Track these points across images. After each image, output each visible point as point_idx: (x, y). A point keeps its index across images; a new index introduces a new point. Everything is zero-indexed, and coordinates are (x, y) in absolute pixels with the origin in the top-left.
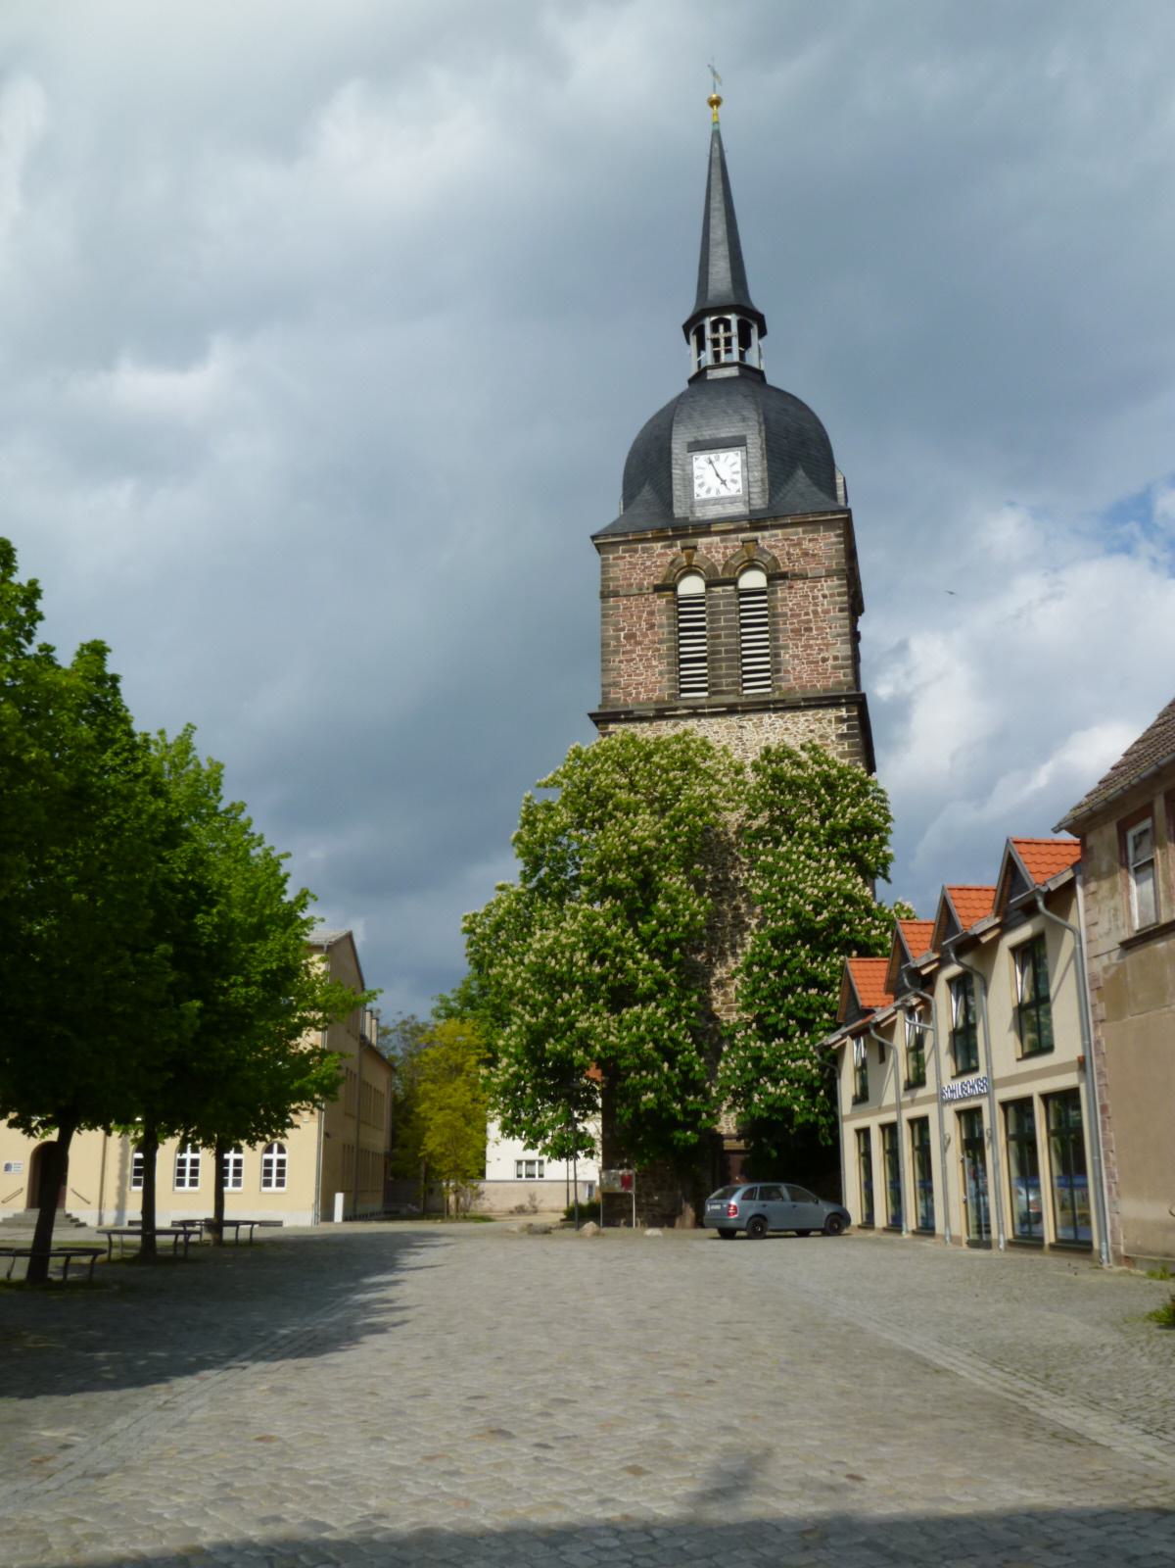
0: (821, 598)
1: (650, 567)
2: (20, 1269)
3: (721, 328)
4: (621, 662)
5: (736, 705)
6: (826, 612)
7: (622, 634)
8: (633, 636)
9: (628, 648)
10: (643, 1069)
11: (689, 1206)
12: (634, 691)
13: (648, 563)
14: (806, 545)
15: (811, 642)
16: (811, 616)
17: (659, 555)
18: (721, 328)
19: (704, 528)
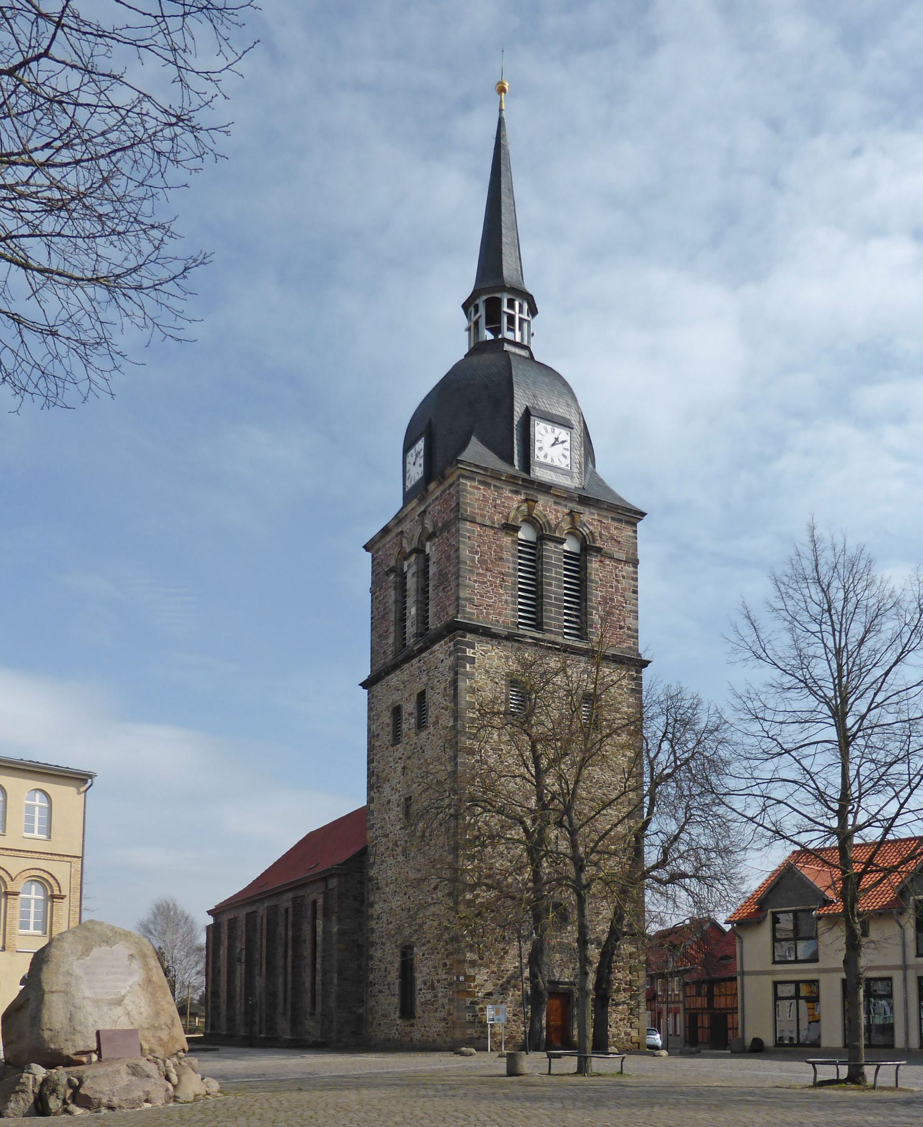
4: (475, 581)
17: (506, 498)
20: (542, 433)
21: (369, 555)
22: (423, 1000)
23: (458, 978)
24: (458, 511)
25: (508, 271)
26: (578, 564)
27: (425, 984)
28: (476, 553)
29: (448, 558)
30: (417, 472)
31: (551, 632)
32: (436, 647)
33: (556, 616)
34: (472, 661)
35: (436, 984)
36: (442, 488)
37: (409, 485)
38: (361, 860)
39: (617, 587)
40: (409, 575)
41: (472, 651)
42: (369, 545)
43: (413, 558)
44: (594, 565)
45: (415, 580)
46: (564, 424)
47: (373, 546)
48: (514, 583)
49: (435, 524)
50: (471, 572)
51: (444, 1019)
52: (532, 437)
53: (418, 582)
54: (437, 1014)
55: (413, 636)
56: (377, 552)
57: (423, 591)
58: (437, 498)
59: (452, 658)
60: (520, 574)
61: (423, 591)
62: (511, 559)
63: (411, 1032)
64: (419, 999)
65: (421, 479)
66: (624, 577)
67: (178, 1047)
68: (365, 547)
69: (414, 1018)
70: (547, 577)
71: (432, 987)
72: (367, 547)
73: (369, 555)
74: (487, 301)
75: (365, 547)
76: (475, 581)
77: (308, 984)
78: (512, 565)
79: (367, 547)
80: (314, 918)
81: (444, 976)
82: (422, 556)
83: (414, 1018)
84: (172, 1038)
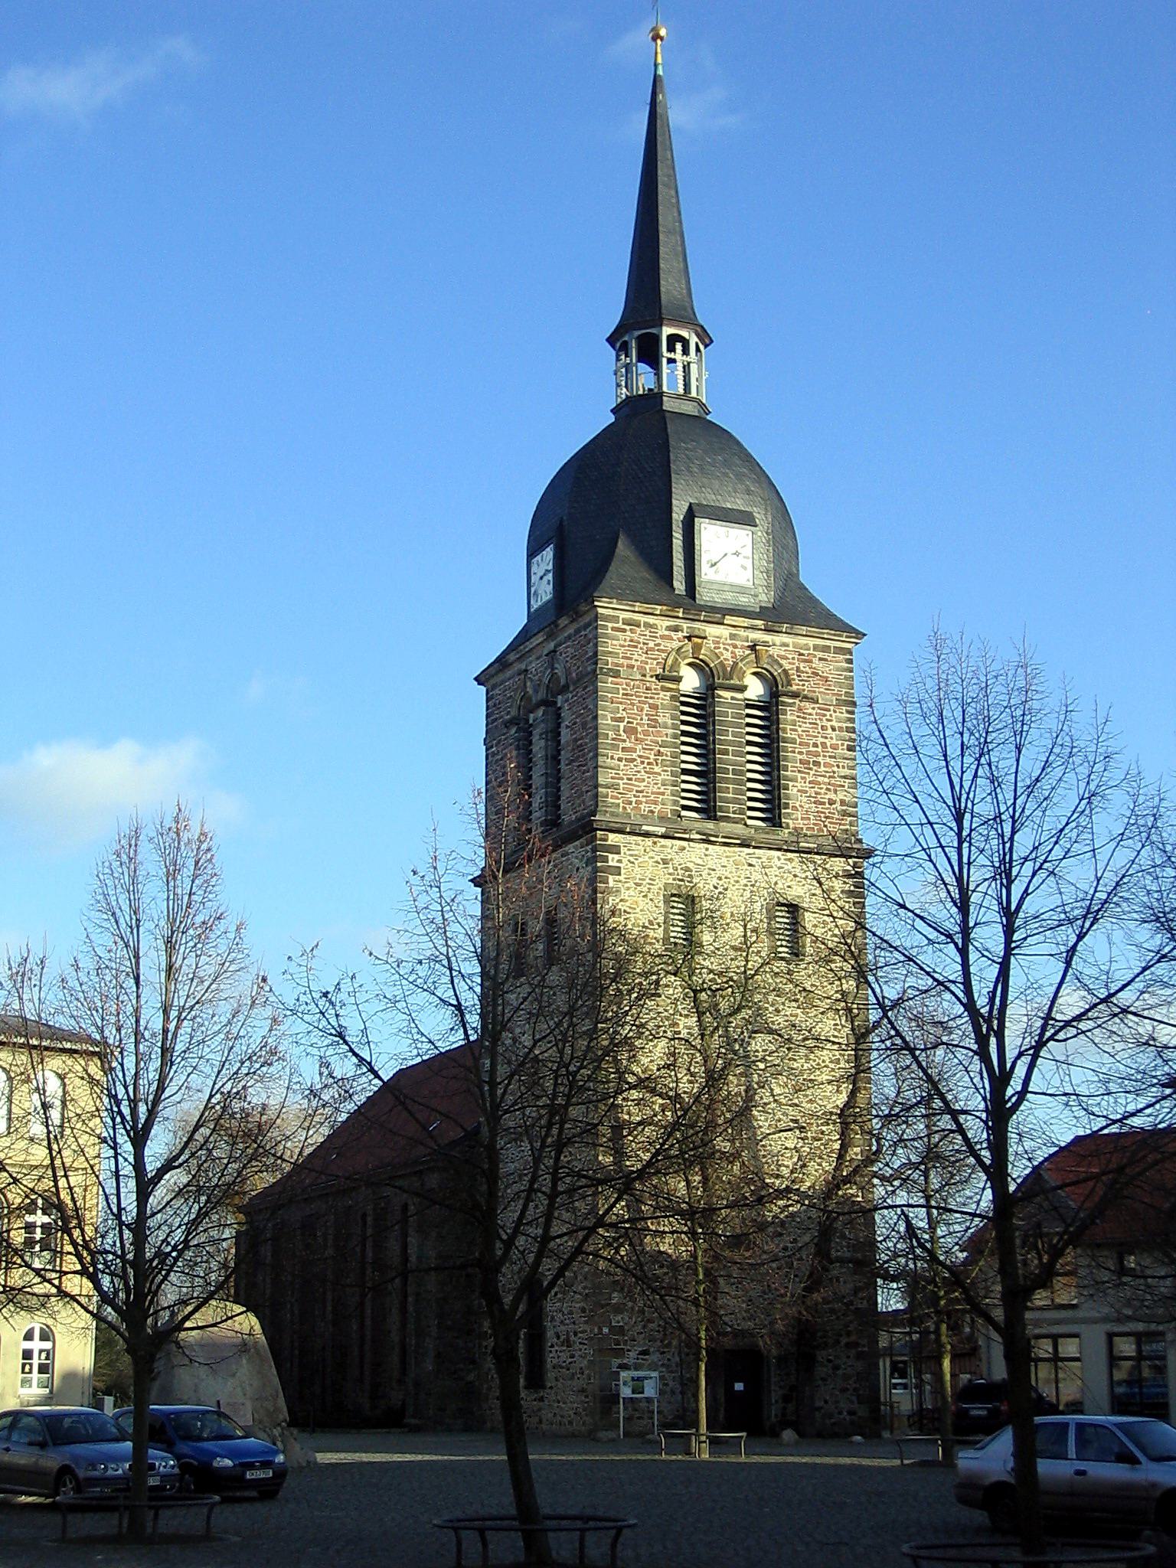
0: (830, 731)
1: (652, 649)
2: (508, 1546)
3: (679, 346)
4: (620, 760)
5: (752, 839)
6: (834, 747)
7: (622, 725)
8: (634, 731)
9: (628, 744)
10: (920, 1340)
11: (45, 758)
12: (634, 799)
13: (651, 644)
14: (816, 663)
15: (820, 779)
16: (819, 749)
17: (662, 637)
18: (679, 346)
19: (718, 614)
20: (712, 537)
21: (483, 689)
22: (555, 1361)
23: (600, 1329)
24: (596, 663)
25: (669, 286)
26: (770, 708)
27: (558, 1337)
28: (621, 720)
29: (584, 725)
30: (545, 591)
31: (727, 819)
32: (570, 848)
33: (739, 787)
34: (617, 871)
35: (572, 1338)
36: (575, 626)
37: (535, 606)
38: (471, 1161)
39: (824, 745)
40: (536, 732)
41: (617, 857)
42: (483, 679)
43: (540, 712)
44: (789, 716)
45: (542, 743)
46: (743, 519)
47: (487, 680)
48: (674, 756)
49: (568, 672)
50: (615, 747)
51: (583, 1390)
52: (697, 548)
53: (546, 747)
54: (575, 1382)
55: (542, 824)
56: (494, 687)
57: (554, 758)
58: (569, 637)
59: (589, 868)
60: (684, 739)
61: (554, 758)
62: (670, 722)
63: (539, 1410)
64: (551, 1359)
65: (549, 602)
66: (834, 729)
67: (281, 1417)
68: (476, 679)
69: (543, 1387)
70: (722, 743)
71: (568, 1343)
72: (478, 680)
73: (483, 689)
74: (639, 339)
75: (476, 679)
76: (620, 760)
77: (395, 1337)
78: (670, 731)
79: (478, 680)
80: (405, 1235)
81: (583, 1327)
82: (551, 709)
83: (543, 1387)
84: (277, 1410)
